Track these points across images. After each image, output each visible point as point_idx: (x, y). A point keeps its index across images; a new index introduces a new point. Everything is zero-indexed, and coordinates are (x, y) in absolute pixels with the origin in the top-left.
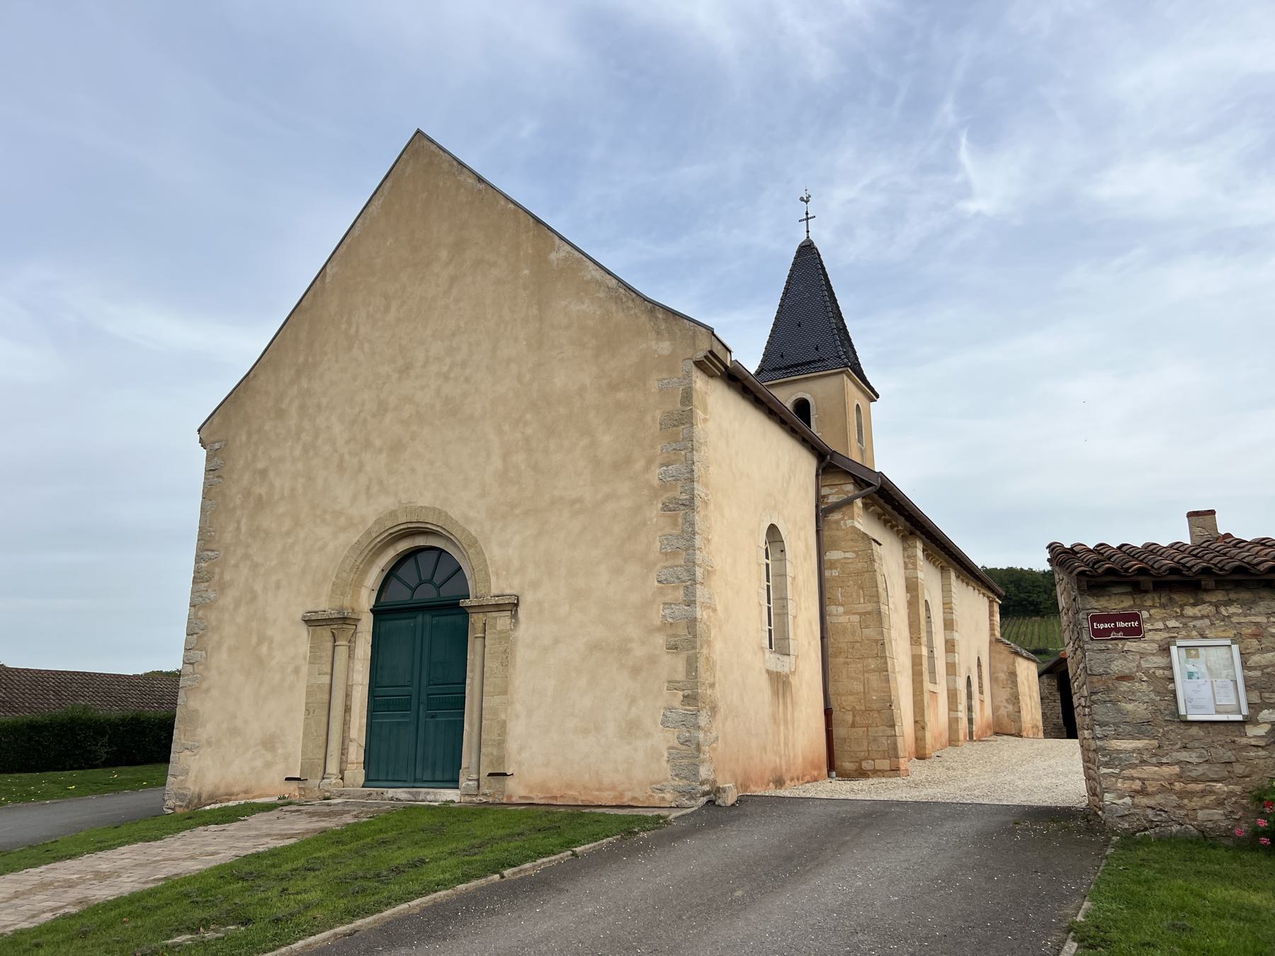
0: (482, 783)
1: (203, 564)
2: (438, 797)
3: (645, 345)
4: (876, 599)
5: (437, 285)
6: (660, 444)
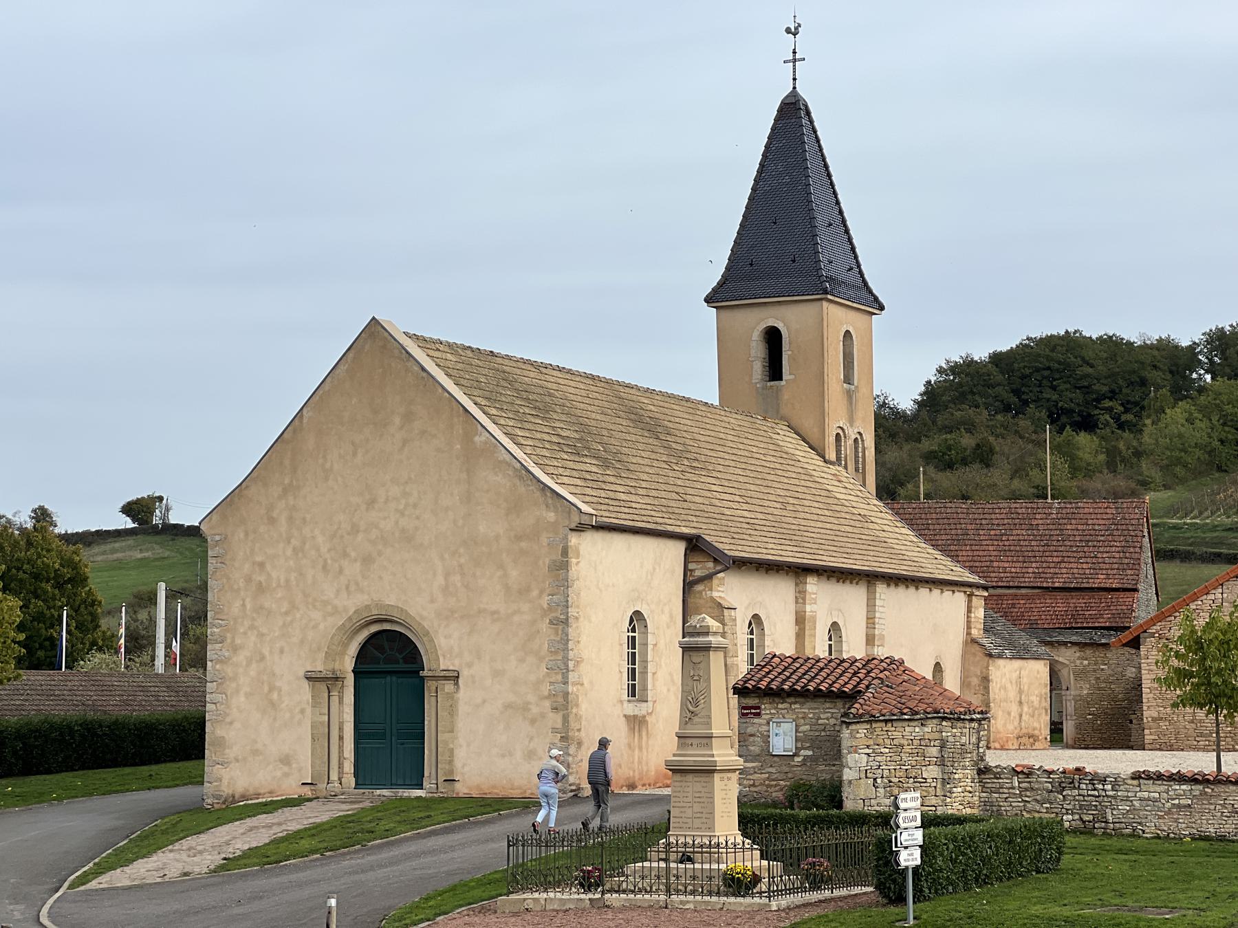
1: (215, 630)
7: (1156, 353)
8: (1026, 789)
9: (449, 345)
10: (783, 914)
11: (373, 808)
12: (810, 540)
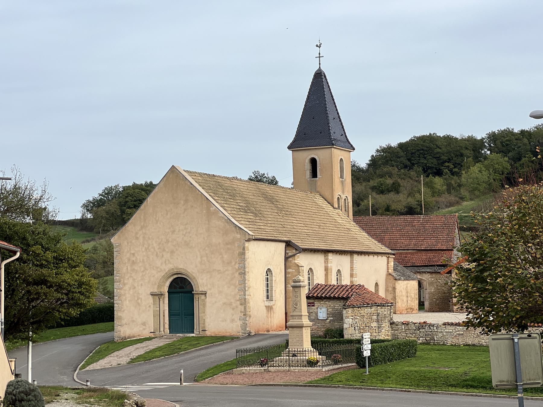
7: (467, 142)
8: (407, 329)
9: (199, 174)
10: (327, 372)
11: (178, 341)
12: (329, 240)
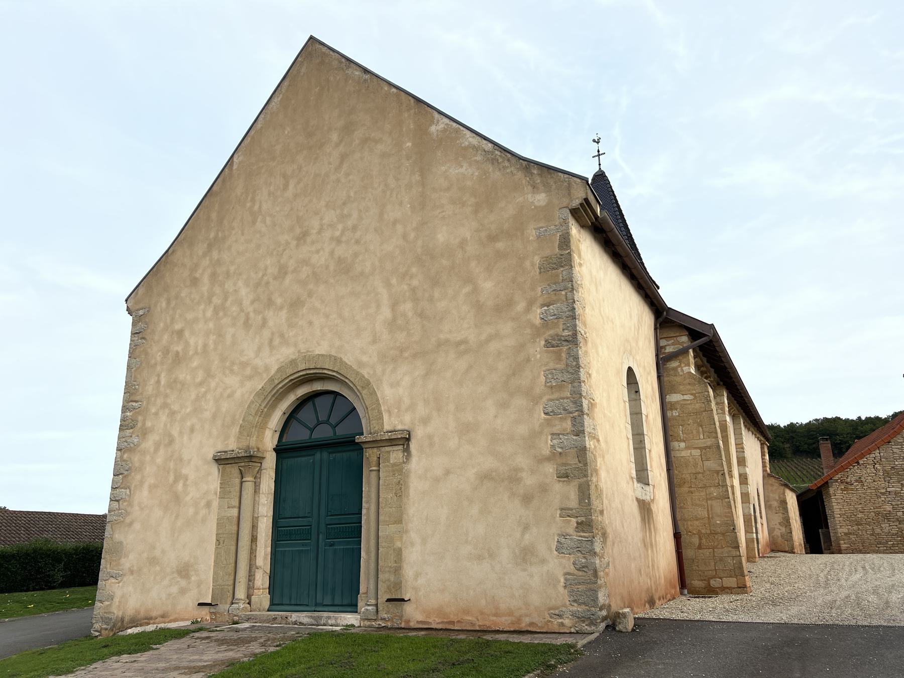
0: (380, 608)
2: (339, 621)
3: (521, 199)
4: (714, 435)
5: (330, 163)
6: (540, 286)
